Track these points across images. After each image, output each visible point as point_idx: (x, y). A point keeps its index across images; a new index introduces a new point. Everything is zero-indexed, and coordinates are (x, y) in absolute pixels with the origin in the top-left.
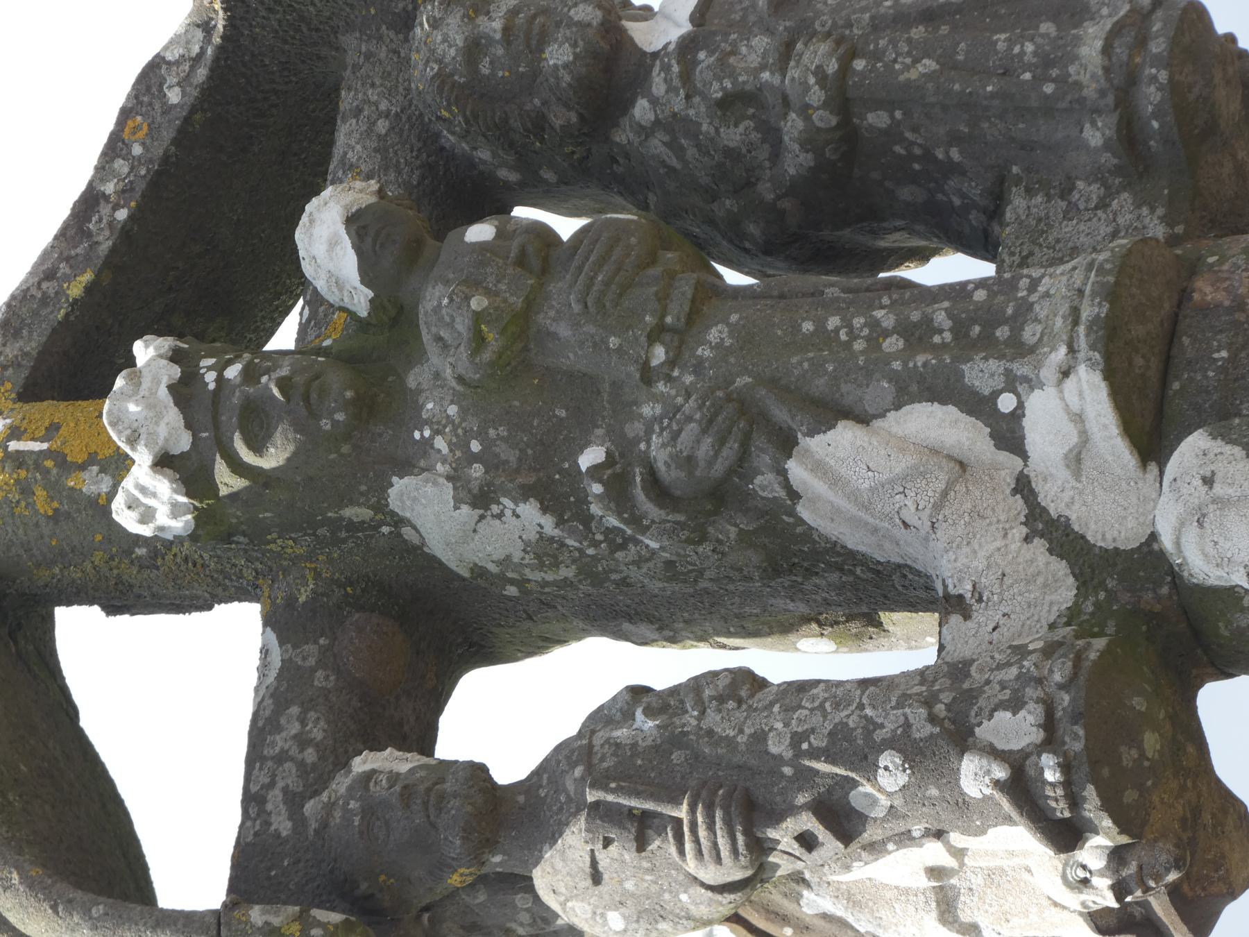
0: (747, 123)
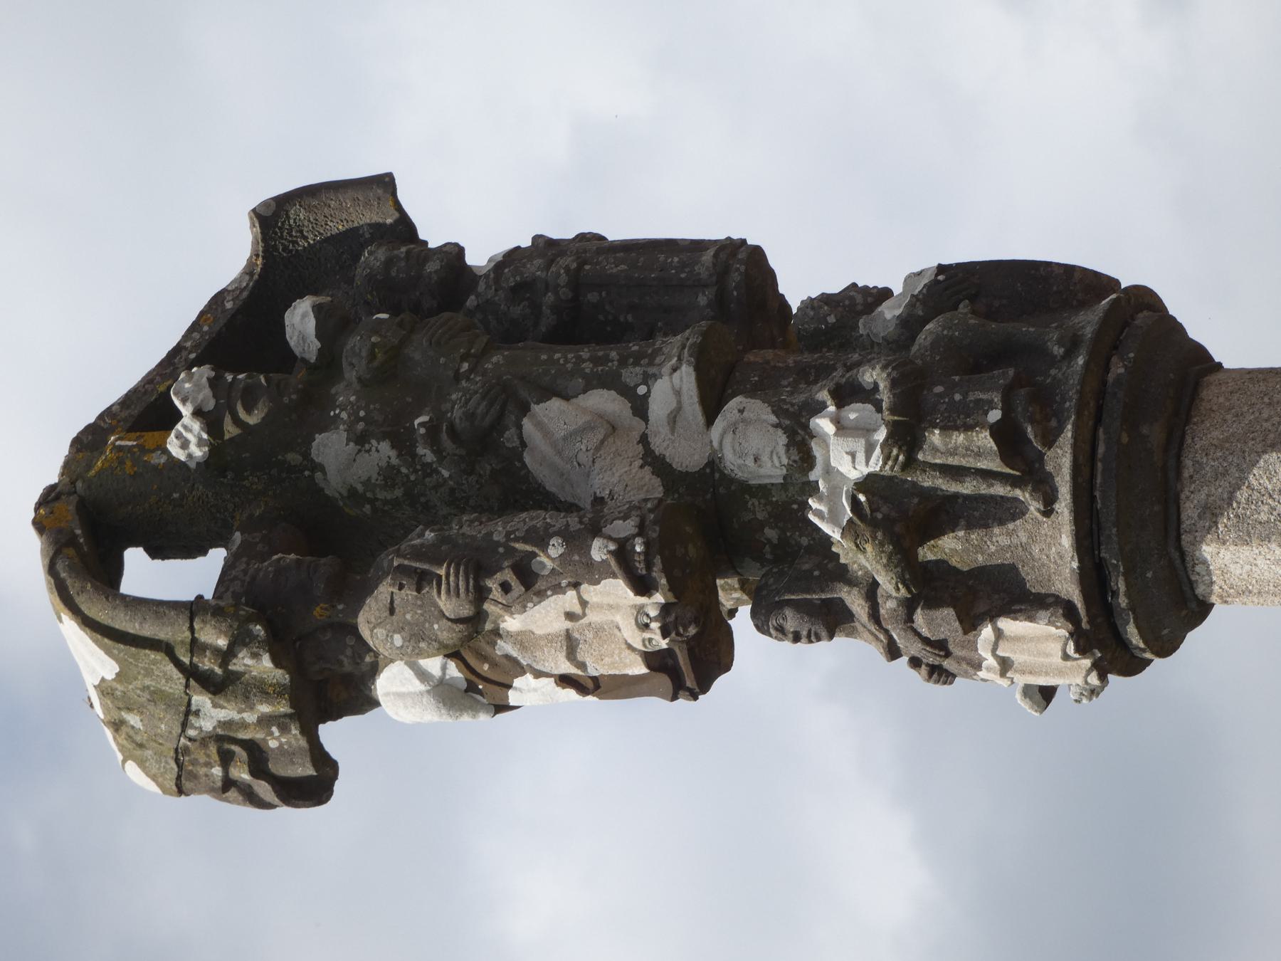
0: (526, 303)
